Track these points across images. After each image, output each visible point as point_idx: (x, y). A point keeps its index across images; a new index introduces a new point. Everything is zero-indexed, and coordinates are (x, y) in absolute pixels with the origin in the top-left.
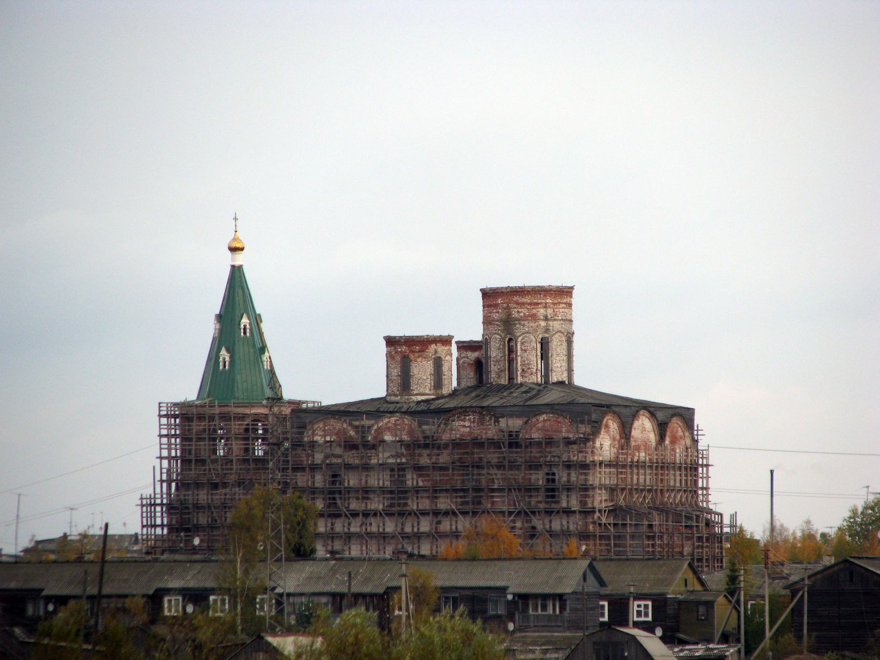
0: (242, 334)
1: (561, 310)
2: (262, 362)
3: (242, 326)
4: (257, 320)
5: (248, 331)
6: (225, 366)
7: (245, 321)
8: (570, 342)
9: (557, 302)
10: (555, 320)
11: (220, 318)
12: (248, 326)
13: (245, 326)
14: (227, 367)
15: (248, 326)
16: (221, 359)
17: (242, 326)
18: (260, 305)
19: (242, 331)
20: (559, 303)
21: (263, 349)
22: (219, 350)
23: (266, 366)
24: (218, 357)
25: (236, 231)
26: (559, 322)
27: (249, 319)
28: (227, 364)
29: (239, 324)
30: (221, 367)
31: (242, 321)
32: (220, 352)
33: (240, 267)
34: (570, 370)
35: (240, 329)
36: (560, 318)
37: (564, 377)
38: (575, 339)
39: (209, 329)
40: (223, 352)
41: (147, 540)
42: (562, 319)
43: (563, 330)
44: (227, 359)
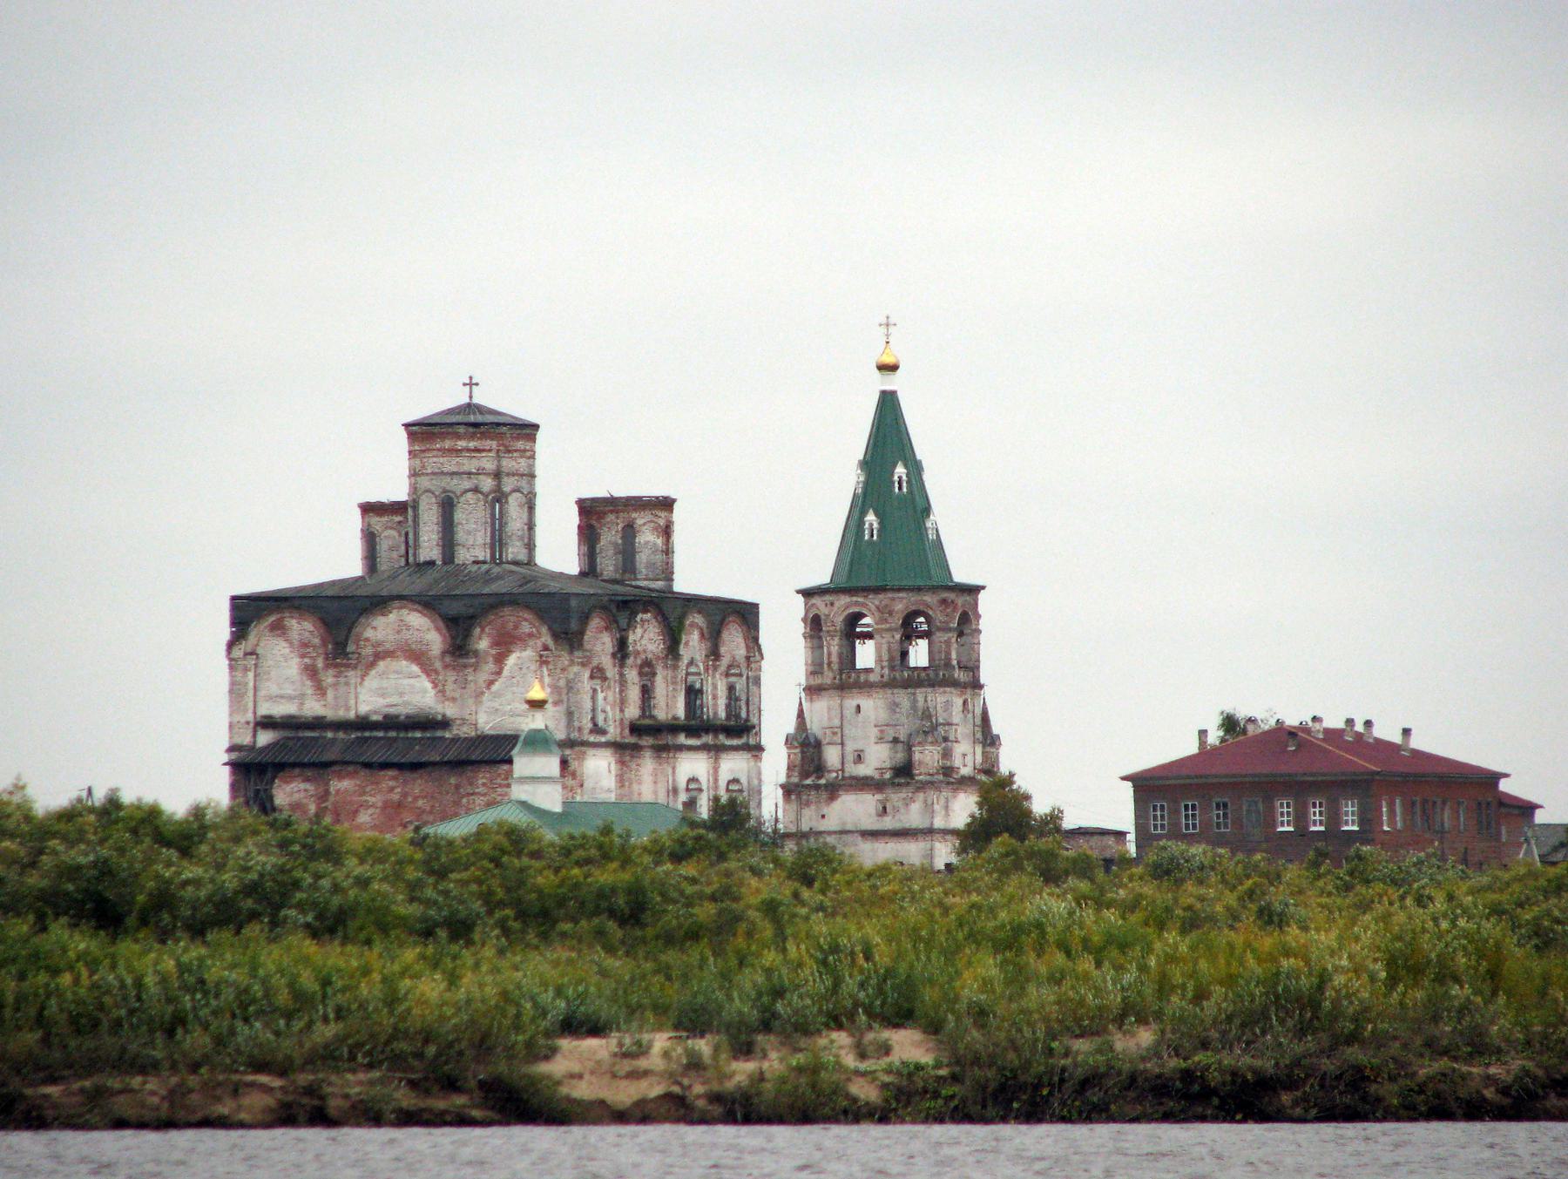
0: (897, 490)
1: (431, 460)
2: (926, 529)
3: (896, 478)
4: (915, 468)
5: (905, 484)
6: (872, 536)
7: (900, 470)
8: (531, 508)
9: (423, 448)
10: (423, 474)
11: (865, 464)
12: (904, 478)
13: (900, 478)
14: (875, 538)
15: (904, 478)
16: (867, 526)
17: (896, 478)
18: (921, 451)
19: (897, 485)
20: (429, 450)
21: (927, 510)
22: (863, 513)
23: (931, 536)
24: (861, 523)
25: (888, 342)
26: (428, 478)
27: (906, 466)
28: (875, 532)
29: (892, 475)
30: (866, 537)
31: (896, 471)
32: (865, 516)
33: (893, 394)
34: (530, 546)
35: (894, 483)
36: (429, 471)
37: (523, 556)
38: (539, 502)
39: (849, 479)
40: (871, 517)
41: (246, 869)
42: (433, 473)
43: (433, 488)
44: (876, 525)
